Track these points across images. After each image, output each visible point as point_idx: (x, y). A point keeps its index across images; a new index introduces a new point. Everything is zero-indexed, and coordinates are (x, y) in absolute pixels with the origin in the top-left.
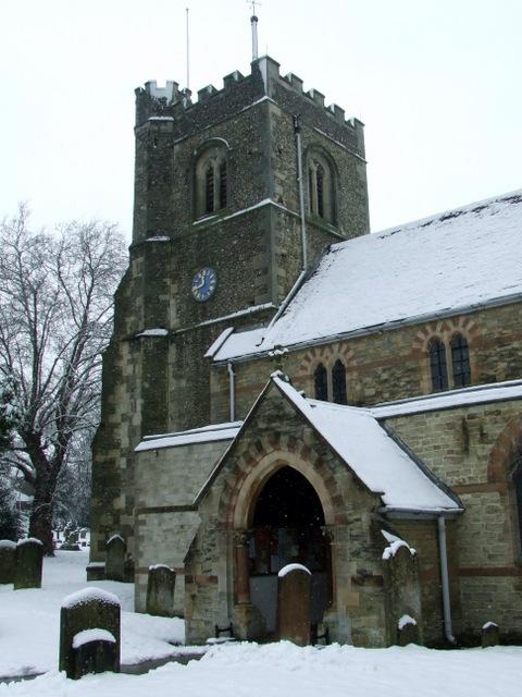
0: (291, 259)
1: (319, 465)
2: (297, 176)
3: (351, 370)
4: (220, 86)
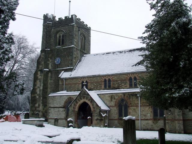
0: (76, 58)
1: (91, 102)
2: (78, 40)
3: (89, 83)
4: (64, 18)
